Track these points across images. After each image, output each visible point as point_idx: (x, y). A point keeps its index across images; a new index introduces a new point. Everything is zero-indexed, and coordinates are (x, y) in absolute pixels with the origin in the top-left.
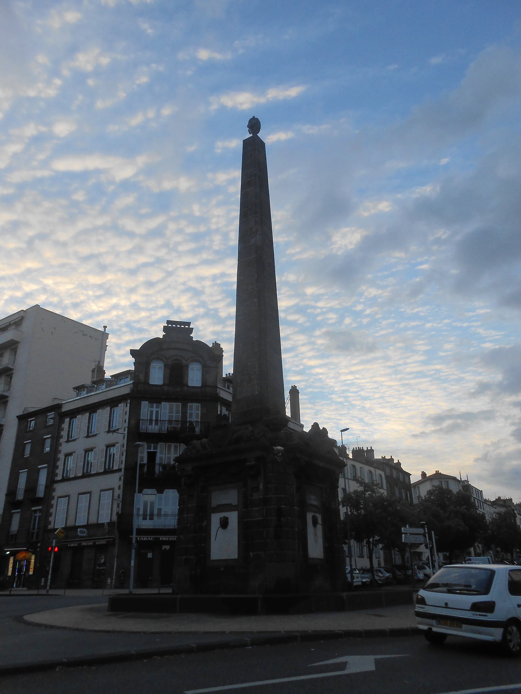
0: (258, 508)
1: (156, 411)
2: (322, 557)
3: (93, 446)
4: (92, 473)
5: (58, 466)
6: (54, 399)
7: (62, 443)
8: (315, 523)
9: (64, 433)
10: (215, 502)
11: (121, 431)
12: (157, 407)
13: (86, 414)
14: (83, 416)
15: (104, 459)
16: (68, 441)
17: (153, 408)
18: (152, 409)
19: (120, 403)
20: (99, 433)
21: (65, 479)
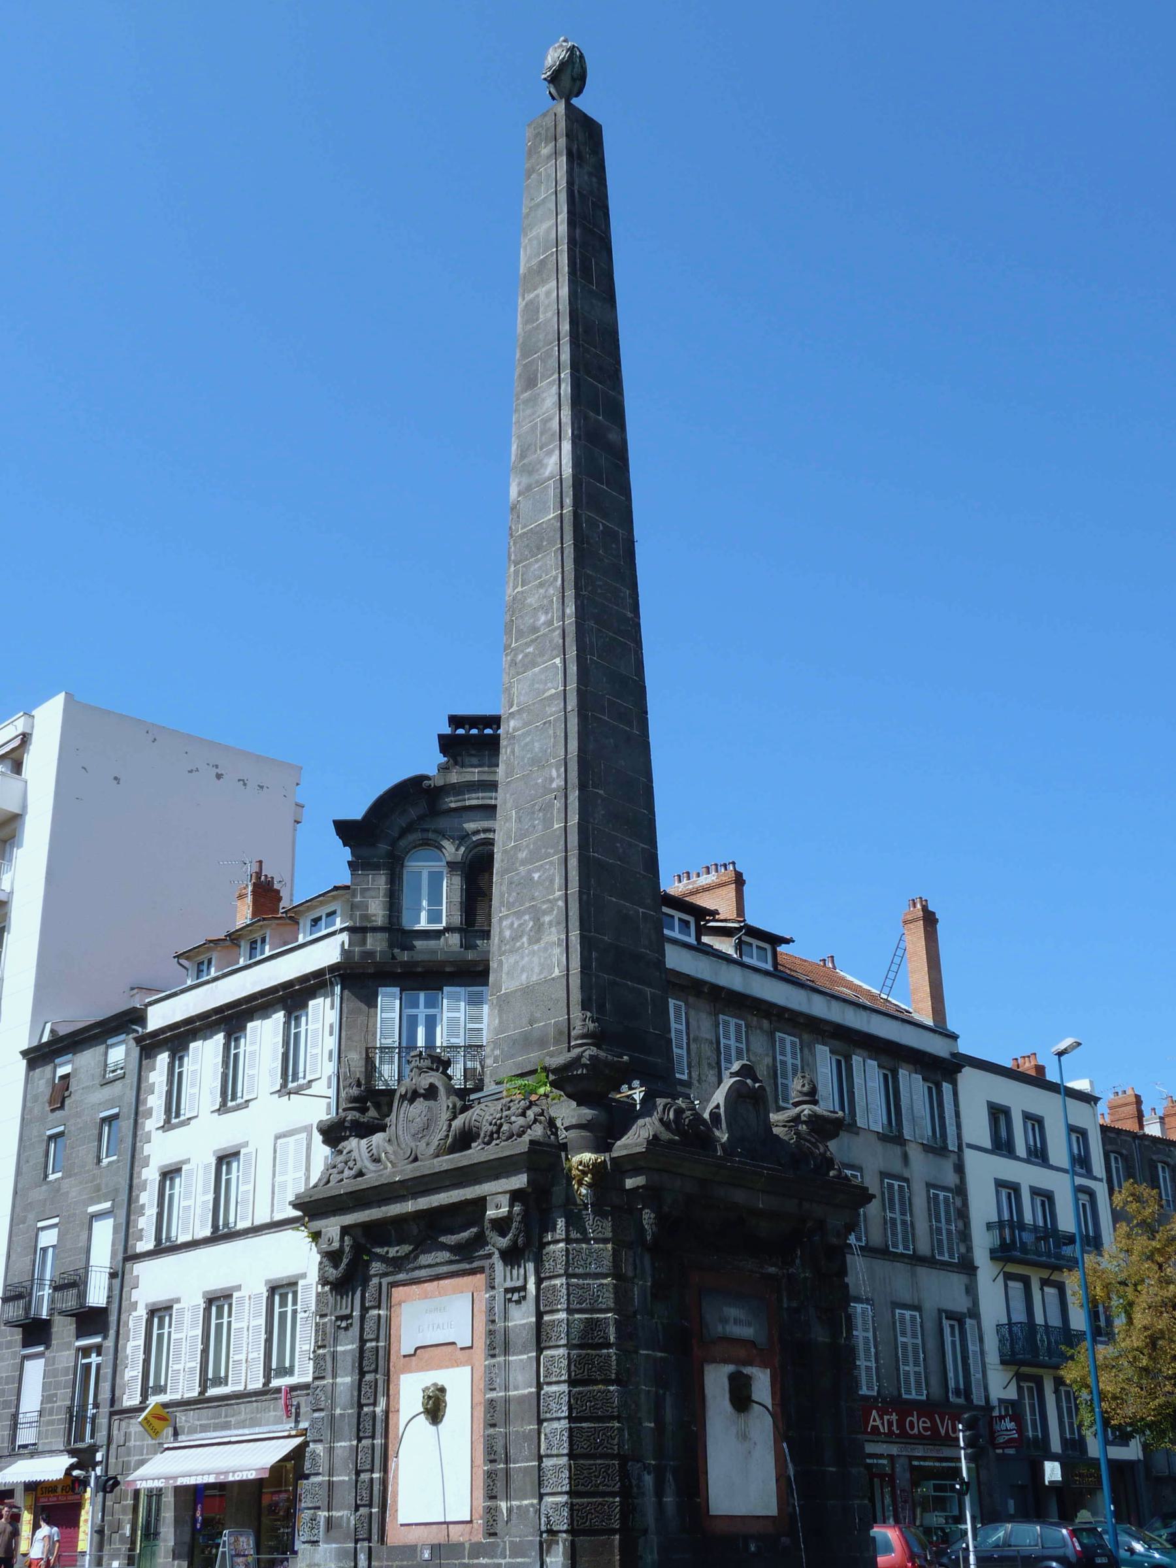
0: (525, 1357)
1: (426, 1015)
2: (773, 1511)
3: (180, 1159)
4: (241, 1225)
5: (143, 1206)
6: (136, 991)
7: (150, 1131)
8: (741, 1399)
9: (156, 1102)
10: (406, 1342)
11: (317, 1089)
12: (428, 1005)
13: (275, 1016)
14: (208, 1042)
15: (211, 1196)
16: (167, 1126)
17: (418, 1007)
18: (413, 1011)
19: (252, 1020)
20: (196, 1115)
21: (164, 1248)
